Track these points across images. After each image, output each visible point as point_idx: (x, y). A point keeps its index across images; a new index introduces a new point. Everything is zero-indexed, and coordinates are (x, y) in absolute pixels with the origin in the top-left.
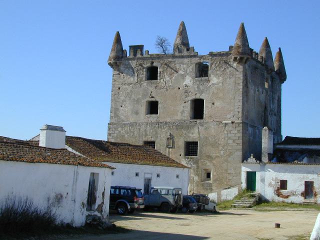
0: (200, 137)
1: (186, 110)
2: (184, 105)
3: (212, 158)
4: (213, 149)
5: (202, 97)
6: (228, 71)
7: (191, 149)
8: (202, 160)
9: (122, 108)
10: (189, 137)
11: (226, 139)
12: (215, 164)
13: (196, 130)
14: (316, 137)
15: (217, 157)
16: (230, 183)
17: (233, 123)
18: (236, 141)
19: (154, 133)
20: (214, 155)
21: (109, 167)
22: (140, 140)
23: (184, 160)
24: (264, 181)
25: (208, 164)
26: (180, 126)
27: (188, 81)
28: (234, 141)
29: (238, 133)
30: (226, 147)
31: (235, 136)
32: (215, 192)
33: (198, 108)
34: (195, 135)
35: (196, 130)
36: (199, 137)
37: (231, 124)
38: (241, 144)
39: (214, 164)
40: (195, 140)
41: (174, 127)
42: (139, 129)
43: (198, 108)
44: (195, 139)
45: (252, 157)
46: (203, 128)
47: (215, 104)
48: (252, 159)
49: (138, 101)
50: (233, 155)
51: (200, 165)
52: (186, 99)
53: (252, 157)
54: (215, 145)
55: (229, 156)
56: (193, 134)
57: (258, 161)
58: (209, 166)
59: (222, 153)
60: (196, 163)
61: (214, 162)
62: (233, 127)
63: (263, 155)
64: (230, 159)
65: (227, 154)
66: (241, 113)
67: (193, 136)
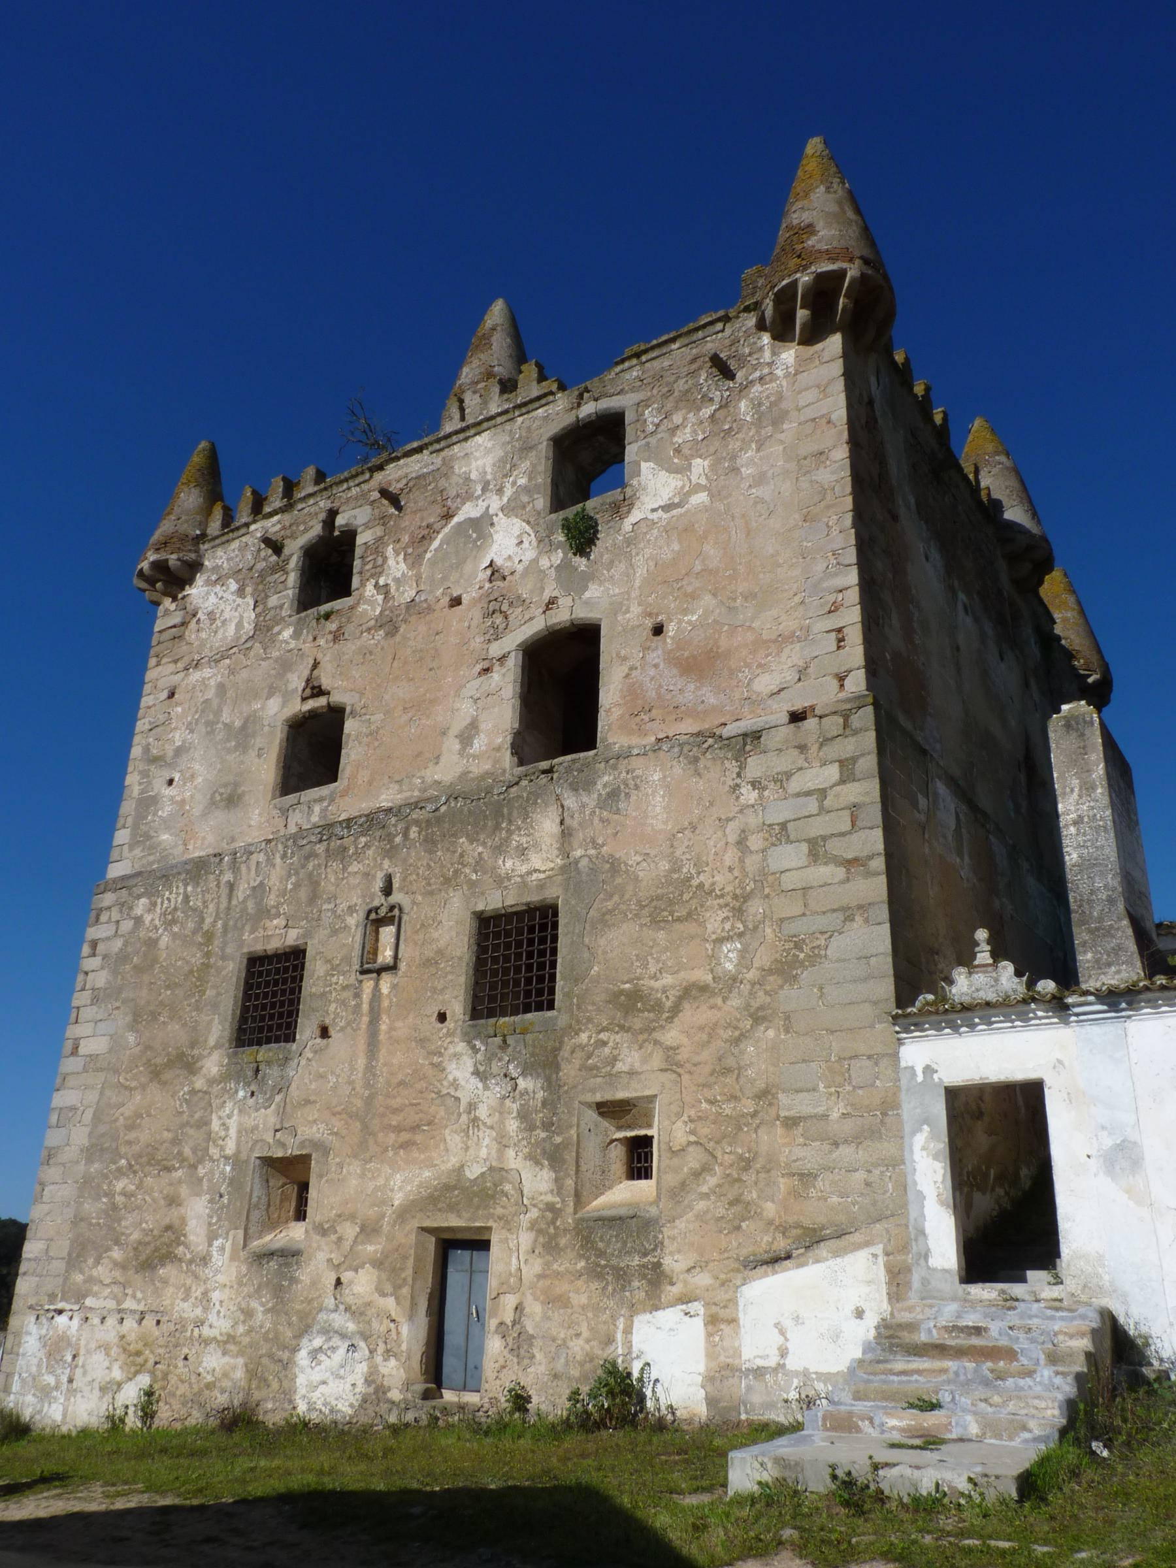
0: (569, 868)
1: (489, 708)
2: (474, 687)
3: (657, 1007)
4: (661, 935)
5: (583, 614)
6: (743, 405)
7: (516, 963)
8: (584, 1037)
9: (168, 791)
10: (500, 881)
11: (755, 842)
12: (683, 1055)
13: (547, 825)
14: (1055, 1178)
15: (692, 992)
16: (812, 1212)
17: (796, 717)
18: (835, 847)
19: (303, 894)
20: (667, 980)
21: (675, 1072)
22: (228, 950)
23: (461, 1047)
24: (1136, 1163)
25: (630, 1059)
26: (480, 810)
27: (513, 542)
28: (817, 850)
29: (842, 781)
30: (756, 908)
31: (822, 810)
32: (685, 1299)
33: (561, 689)
34: (536, 861)
35: (547, 825)
36: (564, 869)
37: (787, 731)
38: (879, 864)
39: (671, 1051)
40: (534, 898)
41: (414, 832)
42: (231, 887)
43: (561, 689)
44: (541, 885)
45: (983, 956)
46: (590, 800)
47: (671, 630)
48: (986, 977)
49: (243, 735)
50: (815, 958)
51: (569, 1071)
52: (496, 650)
53: (983, 956)
54: (673, 904)
55: (786, 969)
56: (522, 852)
57: (1047, 986)
58: (636, 1068)
59: (729, 957)
60: (546, 1064)
61: (672, 1035)
62: (802, 748)
63: (1080, 936)
64: (791, 998)
65: (763, 958)
66: (855, 636)
67: (529, 862)
